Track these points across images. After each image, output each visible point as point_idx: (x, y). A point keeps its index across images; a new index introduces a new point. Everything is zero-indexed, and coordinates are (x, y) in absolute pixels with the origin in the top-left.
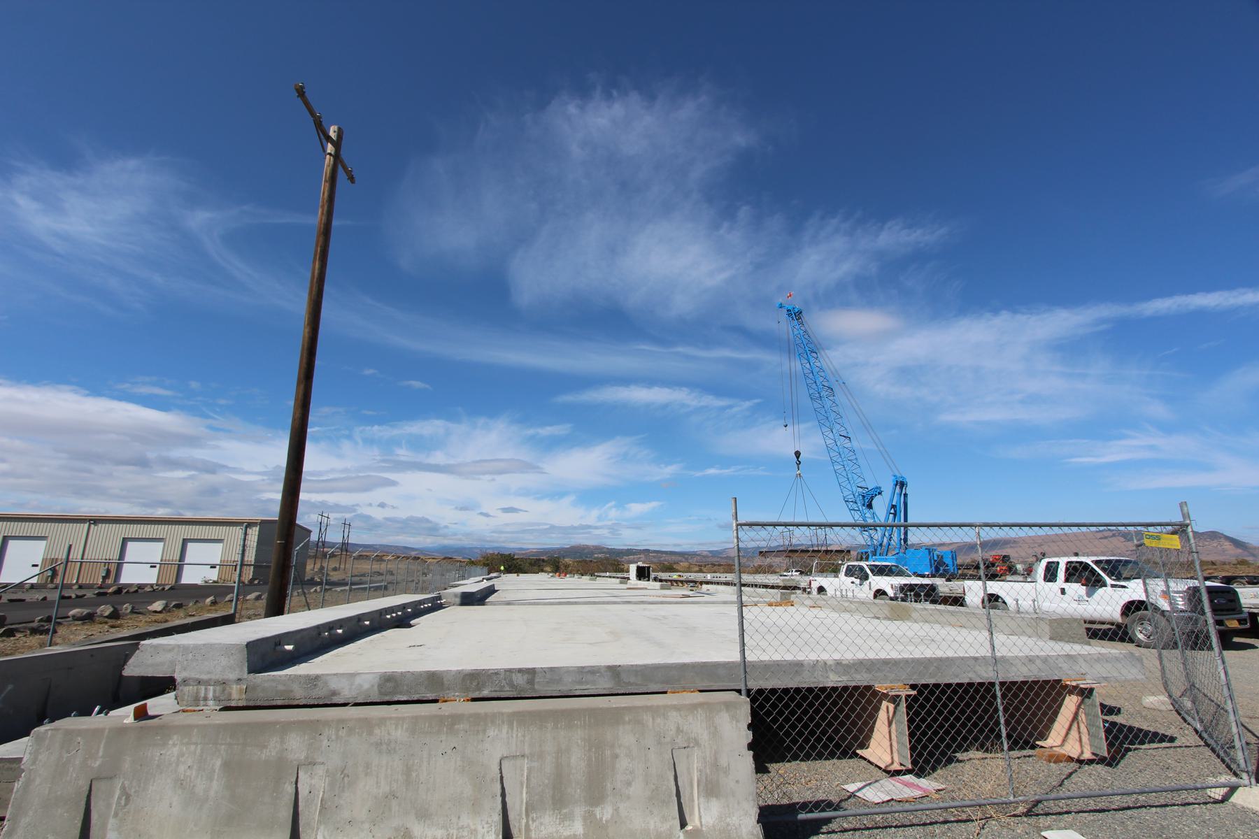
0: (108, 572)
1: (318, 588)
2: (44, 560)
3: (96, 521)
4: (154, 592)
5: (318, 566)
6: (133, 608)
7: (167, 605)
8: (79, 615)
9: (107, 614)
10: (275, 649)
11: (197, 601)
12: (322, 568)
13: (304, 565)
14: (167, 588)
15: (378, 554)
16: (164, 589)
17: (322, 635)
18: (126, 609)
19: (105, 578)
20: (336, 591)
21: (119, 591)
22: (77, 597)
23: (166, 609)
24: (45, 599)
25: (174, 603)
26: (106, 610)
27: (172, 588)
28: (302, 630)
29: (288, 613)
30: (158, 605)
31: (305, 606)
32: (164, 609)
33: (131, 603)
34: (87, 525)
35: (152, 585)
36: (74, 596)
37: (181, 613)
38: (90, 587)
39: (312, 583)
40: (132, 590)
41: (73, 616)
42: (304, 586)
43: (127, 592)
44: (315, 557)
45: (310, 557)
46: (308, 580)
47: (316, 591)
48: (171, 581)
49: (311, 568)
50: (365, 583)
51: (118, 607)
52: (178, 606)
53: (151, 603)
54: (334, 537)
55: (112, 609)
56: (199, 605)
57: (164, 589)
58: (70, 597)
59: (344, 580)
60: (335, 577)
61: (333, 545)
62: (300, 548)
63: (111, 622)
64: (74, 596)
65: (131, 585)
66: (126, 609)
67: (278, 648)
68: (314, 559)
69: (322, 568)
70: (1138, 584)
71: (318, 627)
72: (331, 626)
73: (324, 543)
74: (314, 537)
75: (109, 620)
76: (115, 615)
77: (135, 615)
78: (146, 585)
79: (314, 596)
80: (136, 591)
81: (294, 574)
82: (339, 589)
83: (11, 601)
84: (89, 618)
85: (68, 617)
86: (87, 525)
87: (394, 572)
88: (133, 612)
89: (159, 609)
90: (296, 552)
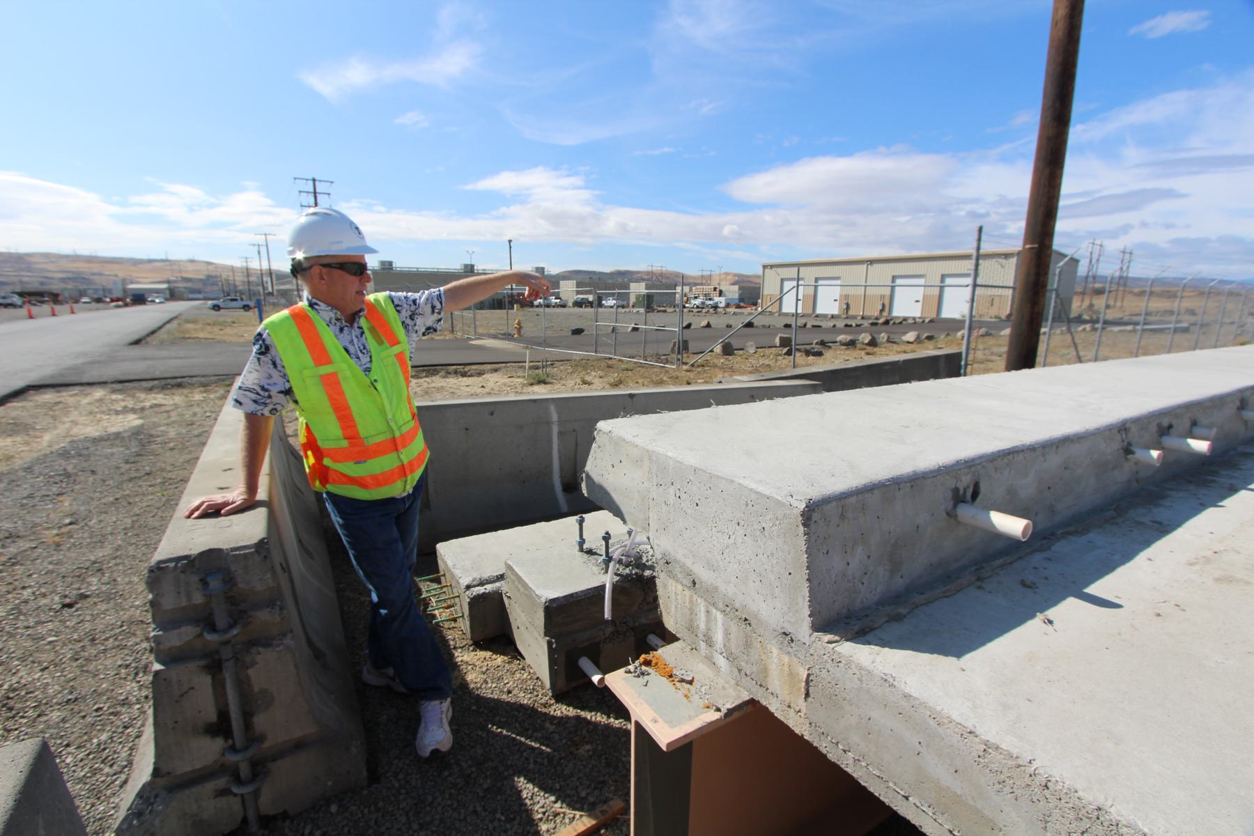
0: (884, 306)
1: (1088, 327)
2: (841, 296)
3: (871, 262)
4: (915, 324)
5: (1086, 303)
6: (889, 337)
7: (918, 337)
8: (844, 341)
9: (866, 341)
10: (951, 515)
11: (948, 334)
12: (1091, 306)
13: (1070, 302)
14: (927, 320)
15: (1166, 289)
16: (923, 322)
17: (1139, 454)
18: (883, 338)
19: (882, 310)
20: (1112, 331)
21: (887, 322)
22: (857, 326)
23: (918, 340)
24: (834, 326)
25: (926, 335)
26: (866, 338)
27: (931, 321)
28: (1066, 441)
29: (1044, 365)
30: (911, 336)
31: (1070, 346)
32: (915, 340)
33: (886, 332)
34: (865, 266)
35: (914, 319)
36: (854, 325)
37: (930, 344)
38: (869, 318)
39: (1079, 320)
40: (898, 321)
41: (840, 342)
42: (1071, 324)
43: (894, 323)
44: (1083, 293)
45: (1076, 293)
46: (1075, 318)
47: (1084, 329)
48: (933, 315)
49: (1077, 306)
50: (1169, 323)
51: (876, 336)
52: (930, 338)
53: (905, 333)
54: (1108, 269)
55: (870, 338)
56: (949, 338)
57: (923, 322)
58: (851, 326)
59: (1121, 319)
60: (1110, 315)
61: (1103, 279)
62: (1065, 264)
63: (869, 349)
64: (854, 325)
65: (899, 317)
66: (883, 338)
67: (966, 513)
68: (1081, 296)
69: (1091, 306)
70: (254, 312)
71: (1123, 428)
72: (1165, 422)
73: (1094, 277)
74: (1082, 270)
75: (868, 347)
76: (873, 343)
77: (890, 344)
78: (909, 318)
79: (1083, 335)
80: (901, 323)
81: (1056, 302)
82: (1116, 329)
83: (814, 326)
84: (851, 344)
85: (836, 342)
86: (865, 266)
87: (1197, 311)
88: (889, 341)
89: (912, 340)
90: (1057, 271)
